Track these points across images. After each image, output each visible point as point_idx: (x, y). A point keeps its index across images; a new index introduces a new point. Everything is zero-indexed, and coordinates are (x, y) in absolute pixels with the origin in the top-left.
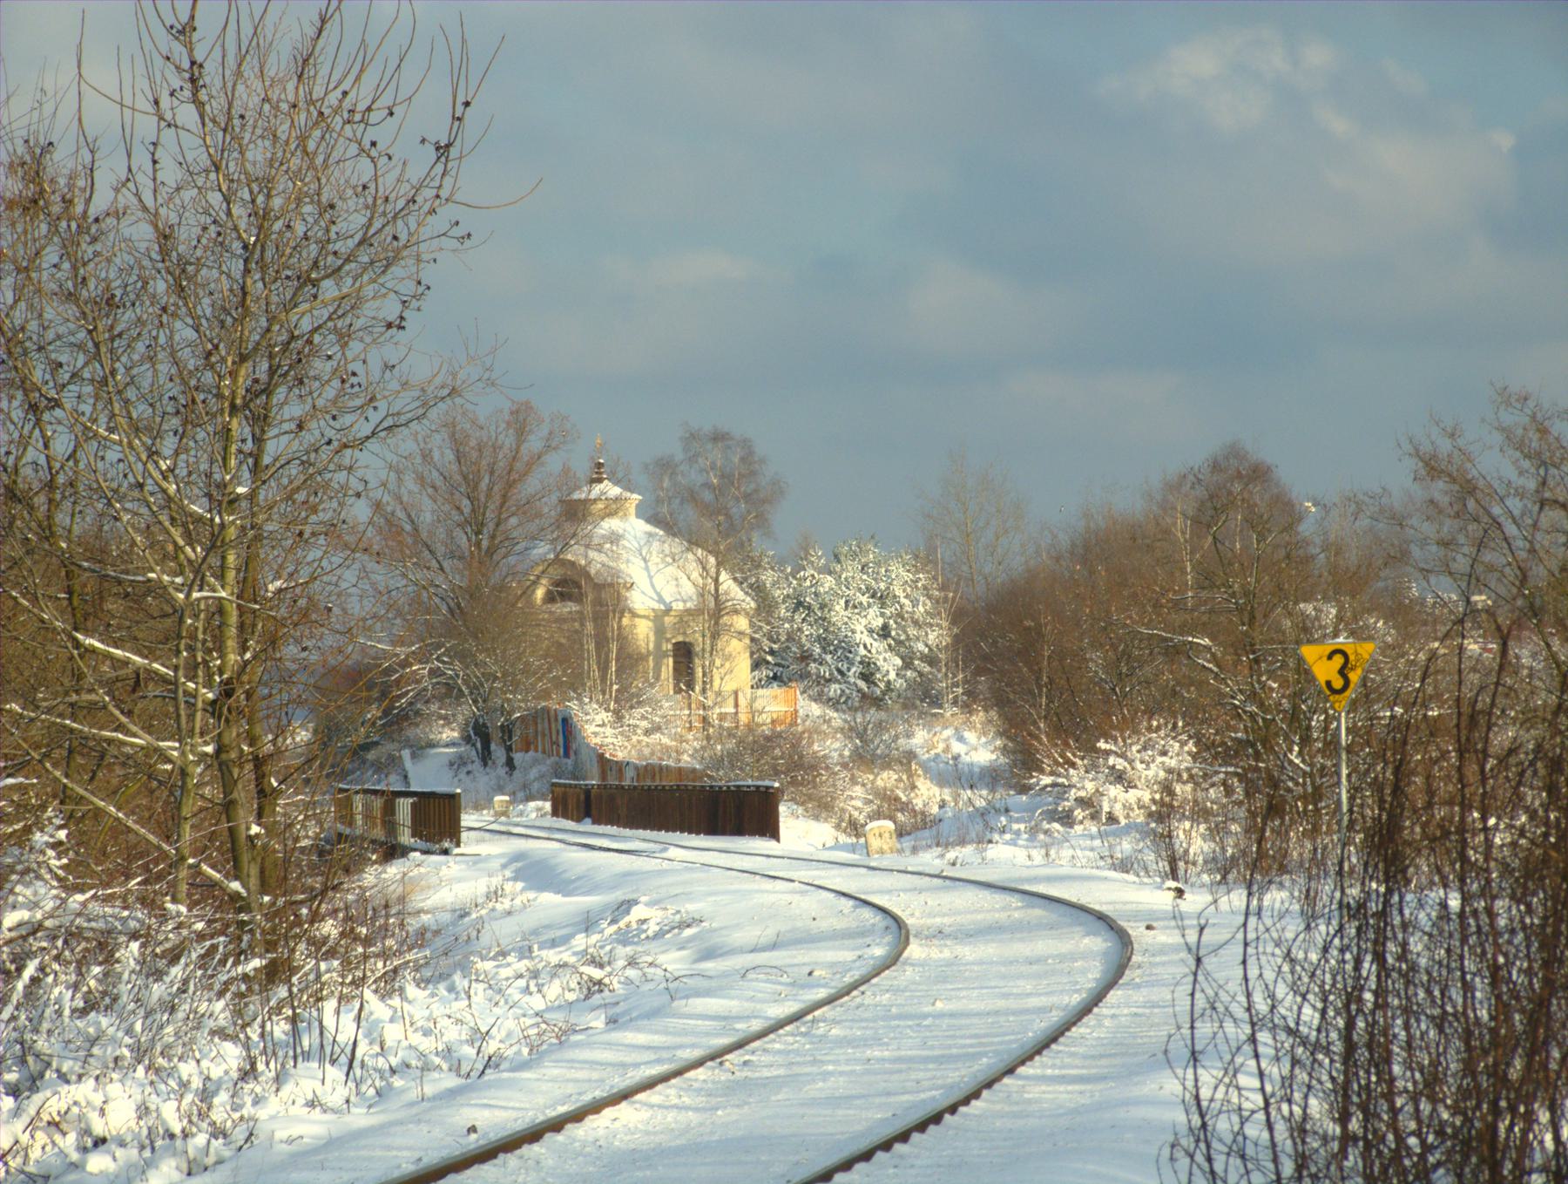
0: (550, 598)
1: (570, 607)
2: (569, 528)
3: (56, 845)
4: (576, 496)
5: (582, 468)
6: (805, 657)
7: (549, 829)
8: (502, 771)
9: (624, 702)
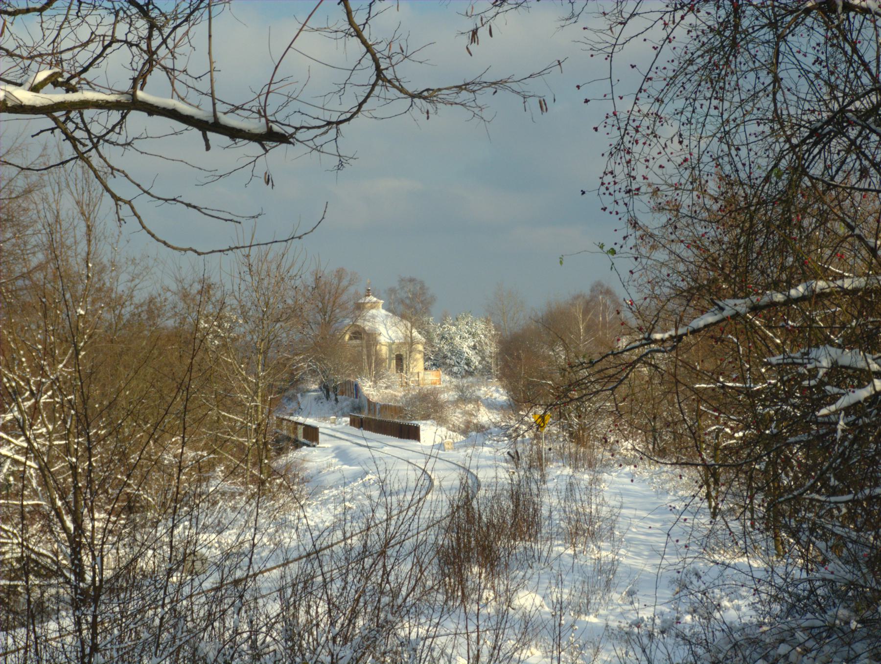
0: (350, 338)
1: (358, 342)
2: (357, 312)
3: (222, 471)
4: (360, 301)
5: (362, 291)
6: (445, 357)
7: (348, 434)
8: (333, 402)
9: (377, 377)
